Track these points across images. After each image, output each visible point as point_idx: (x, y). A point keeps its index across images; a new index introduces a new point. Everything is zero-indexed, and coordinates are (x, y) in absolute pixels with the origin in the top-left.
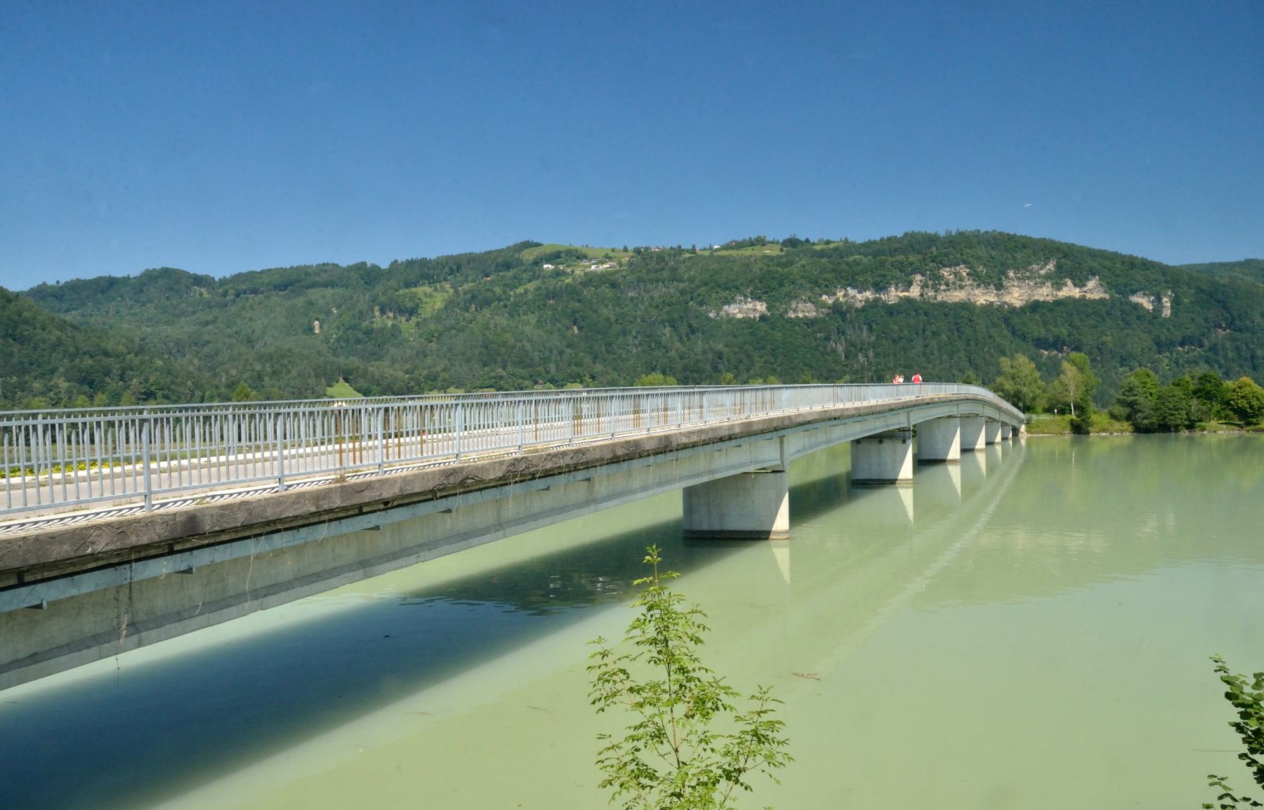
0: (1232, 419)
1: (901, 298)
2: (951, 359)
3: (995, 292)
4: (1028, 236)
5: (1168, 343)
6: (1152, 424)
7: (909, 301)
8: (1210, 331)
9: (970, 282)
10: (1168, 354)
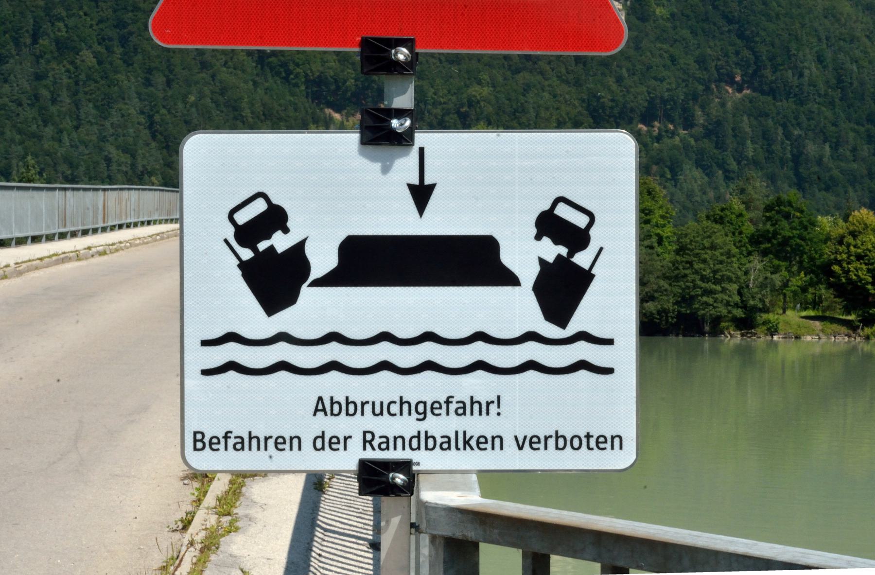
0: (828, 308)
5: (616, 111)
6: (663, 312)
8: (708, 89)
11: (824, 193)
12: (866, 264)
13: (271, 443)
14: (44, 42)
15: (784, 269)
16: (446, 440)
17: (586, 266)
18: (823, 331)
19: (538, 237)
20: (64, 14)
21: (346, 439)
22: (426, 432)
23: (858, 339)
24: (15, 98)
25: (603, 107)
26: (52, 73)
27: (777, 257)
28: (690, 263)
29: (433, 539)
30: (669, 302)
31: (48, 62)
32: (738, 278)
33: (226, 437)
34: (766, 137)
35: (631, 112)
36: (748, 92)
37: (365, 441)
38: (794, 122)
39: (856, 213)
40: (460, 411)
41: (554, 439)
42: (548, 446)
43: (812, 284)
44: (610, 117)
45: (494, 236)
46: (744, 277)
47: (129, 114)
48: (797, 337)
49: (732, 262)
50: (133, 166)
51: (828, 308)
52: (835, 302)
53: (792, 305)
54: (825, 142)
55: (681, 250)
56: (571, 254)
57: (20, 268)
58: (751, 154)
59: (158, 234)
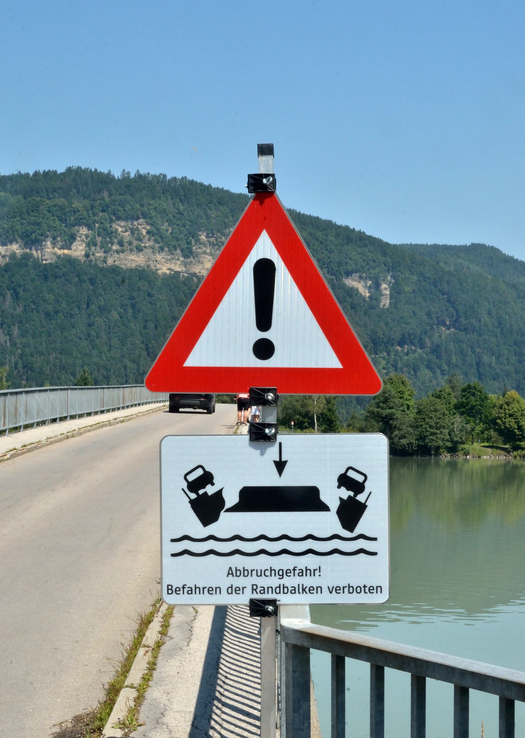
1: (59, 257)
2: (123, 345)
3: (182, 259)
4: (225, 189)
5: (385, 340)
7: (70, 261)
8: (432, 328)
9: (151, 243)
10: (385, 354)
11: (492, 381)
12: (514, 419)
13: (206, 590)
14: (92, 307)
15: (472, 422)
16: (293, 588)
17: (363, 502)
18: (492, 453)
19: (339, 487)
20: (103, 293)
21: (243, 588)
22: (284, 585)
23: (510, 458)
24: (78, 336)
25: (379, 338)
26: (97, 322)
27: (468, 415)
28: (424, 419)
29: (287, 645)
30: (413, 439)
31: (95, 317)
32: (448, 426)
33: (183, 588)
34: (462, 352)
35: (393, 340)
36: (453, 330)
37: (253, 589)
38: (477, 345)
39: (509, 393)
40: (301, 574)
41: (347, 588)
42: (345, 591)
43: (486, 429)
44: (382, 343)
45: (317, 486)
46: (451, 426)
47: (136, 344)
48: (479, 457)
49: (446, 418)
50: (138, 370)
51: (495, 441)
52: (499, 439)
53: (476, 440)
54: (493, 355)
55: (419, 412)
56: (355, 495)
57: (81, 431)
58: (455, 361)
59: (151, 410)
